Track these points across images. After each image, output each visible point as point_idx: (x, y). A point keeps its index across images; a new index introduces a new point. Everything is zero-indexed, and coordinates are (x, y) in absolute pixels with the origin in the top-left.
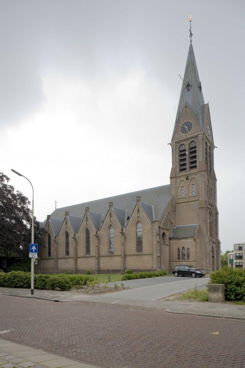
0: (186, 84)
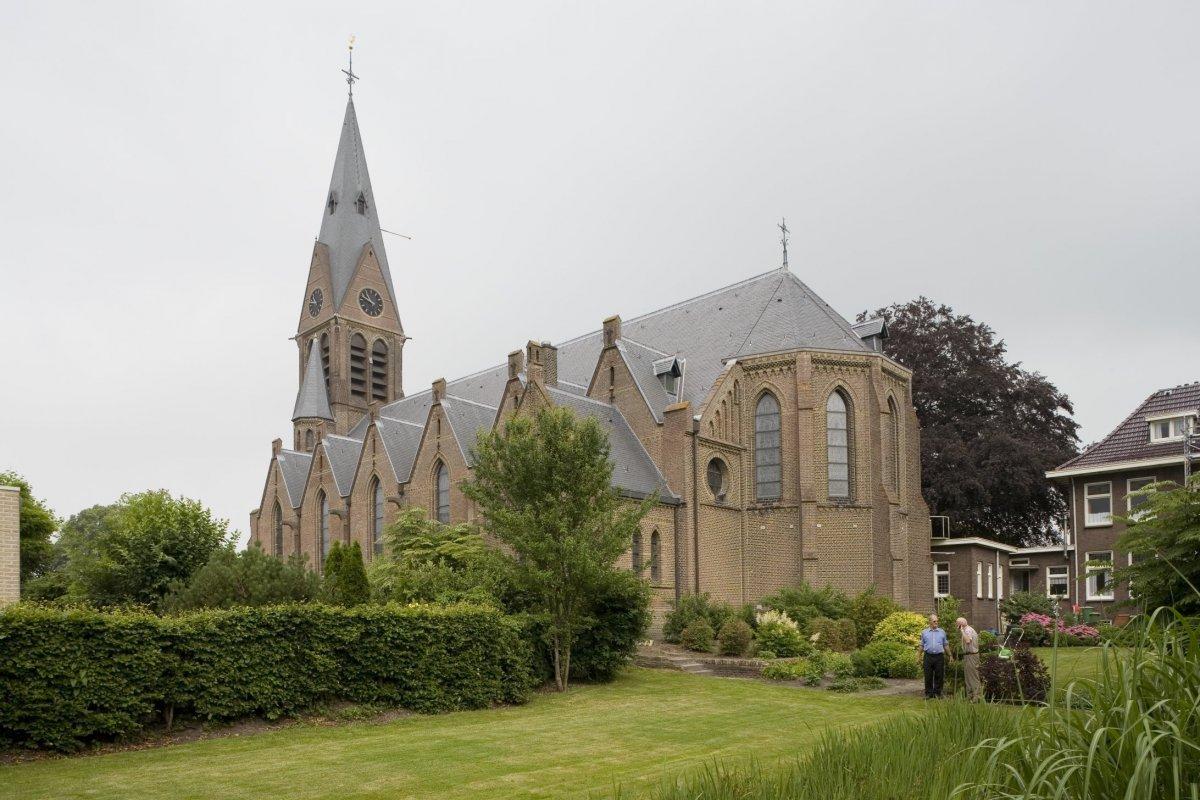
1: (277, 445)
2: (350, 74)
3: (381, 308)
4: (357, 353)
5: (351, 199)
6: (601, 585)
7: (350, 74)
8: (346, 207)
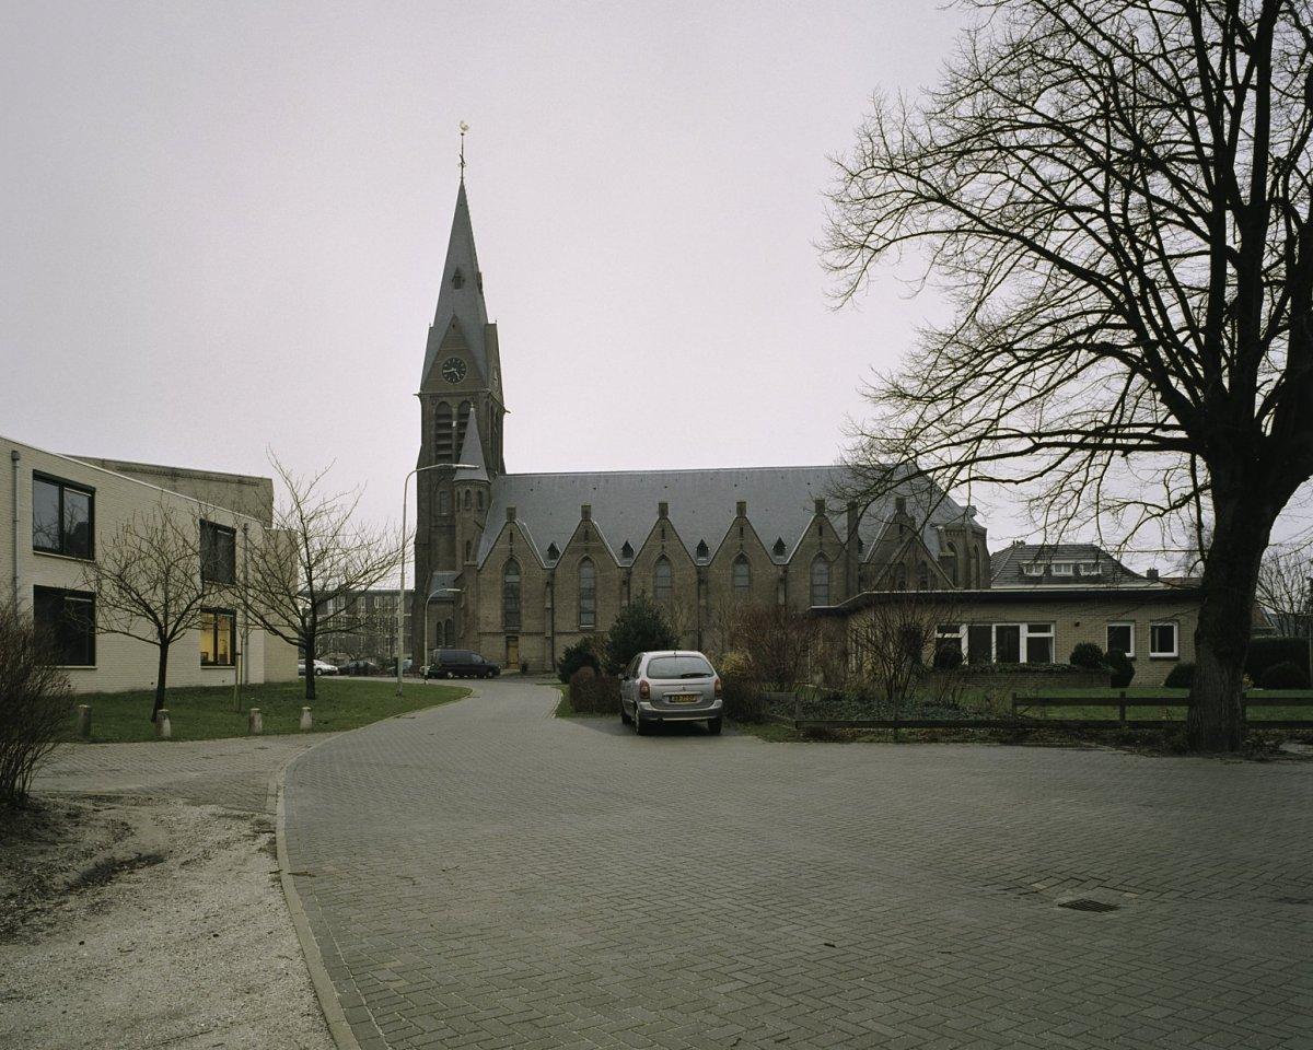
5: (462, 277)
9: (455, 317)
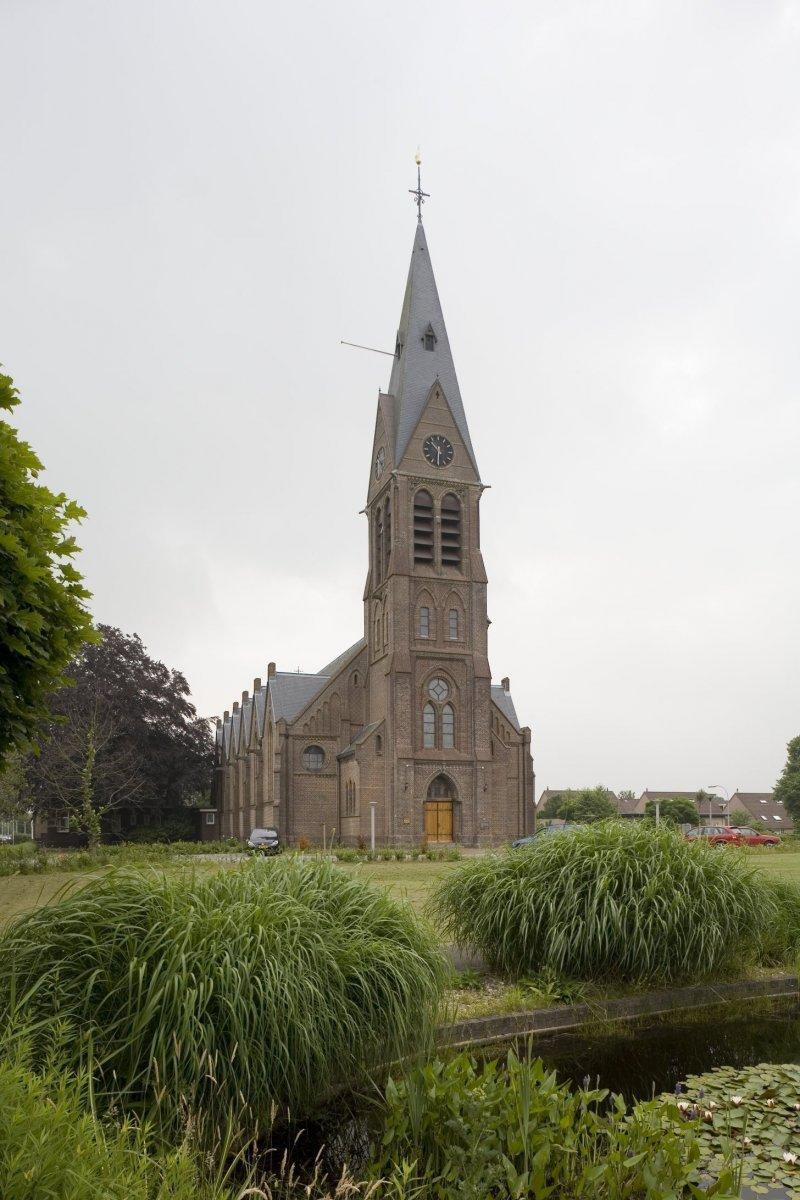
0: (437, 347)
1: (257, 682)
2: (419, 193)
3: (451, 456)
4: (423, 509)
5: (423, 336)
6: (655, 1018)
7: (419, 193)
8: (415, 345)
9: (437, 384)
